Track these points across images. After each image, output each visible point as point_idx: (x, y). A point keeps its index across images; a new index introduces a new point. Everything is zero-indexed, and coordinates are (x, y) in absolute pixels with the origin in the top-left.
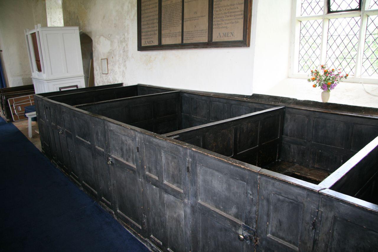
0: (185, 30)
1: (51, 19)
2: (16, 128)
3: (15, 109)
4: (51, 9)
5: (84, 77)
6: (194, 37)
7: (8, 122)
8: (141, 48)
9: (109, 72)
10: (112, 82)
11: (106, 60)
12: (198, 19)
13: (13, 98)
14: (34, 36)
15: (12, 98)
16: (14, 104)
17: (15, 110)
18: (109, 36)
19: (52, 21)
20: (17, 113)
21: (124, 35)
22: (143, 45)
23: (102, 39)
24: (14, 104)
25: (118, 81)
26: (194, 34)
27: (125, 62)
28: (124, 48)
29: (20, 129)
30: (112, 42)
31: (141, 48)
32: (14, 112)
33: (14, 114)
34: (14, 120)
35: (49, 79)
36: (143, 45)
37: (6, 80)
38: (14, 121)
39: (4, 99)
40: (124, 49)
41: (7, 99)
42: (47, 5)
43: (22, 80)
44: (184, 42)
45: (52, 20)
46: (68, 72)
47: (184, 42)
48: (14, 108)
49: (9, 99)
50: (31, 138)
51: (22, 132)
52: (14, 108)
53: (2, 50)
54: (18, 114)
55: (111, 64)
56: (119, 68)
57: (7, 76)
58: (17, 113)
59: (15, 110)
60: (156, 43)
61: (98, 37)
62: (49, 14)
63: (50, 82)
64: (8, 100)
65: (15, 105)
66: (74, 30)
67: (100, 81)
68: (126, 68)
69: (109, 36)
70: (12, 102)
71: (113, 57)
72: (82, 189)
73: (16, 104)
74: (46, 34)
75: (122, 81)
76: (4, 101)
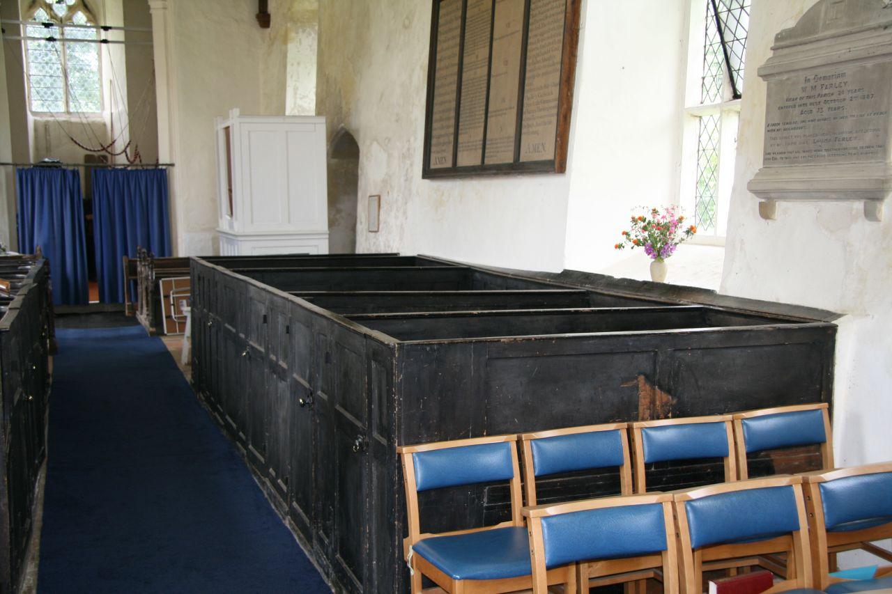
0: (488, 137)
1: (296, 89)
2: (165, 347)
3: (173, 305)
4: (299, 64)
5: (327, 236)
6: (498, 152)
7: (152, 333)
8: (429, 173)
9: (381, 226)
10: (382, 249)
11: (377, 198)
12: (505, 114)
13: (173, 279)
14: (227, 129)
15: (170, 279)
16: (171, 292)
17: (172, 307)
18: (387, 141)
19: (298, 96)
20: (175, 314)
21: (409, 141)
22: (432, 167)
23: (375, 146)
24: (173, 294)
25: (392, 249)
26: (499, 145)
27: (406, 203)
28: (407, 170)
29: (171, 348)
30: (390, 155)
31: (429, 173)
32: (168, 310)
33: (169, 317)
34: (166, 332)
35: (243, 234)
36: (432, 167)
37: (174, 237)
38: (166, 335)
39: (152, 278)
40: (406, 175)
41: (158, 278)
42: (289, 55)
43: (210, 243)
44: (487, 162)
45: (299, 92)
46: (289, 222)
47: (487, 162)
48: (172, 302)
49: (163, 279)
50: (186, 364)
51: (172, 354)
52: (172, 302)
53: (174, 162)
54: (179, 318)
55: (385, 208)
56: (396, 217)
57: (176, 227)
58: (176, 316)
59: (172, 307)
60: (449, 164)
61: (368, 142)
62: (292, 76)
63: (244, 241)
64: (161, 282)
65: (175, 296)
66: (315, 124)
67: (366, 245)
68: (406, 218)
69: (387, 141)
70: (168, 286)
71: (388, 193)
72: (224, 432)
73: (177, 293)
74: (249, 132)
75: (398, 249)
76: (152, 282)
